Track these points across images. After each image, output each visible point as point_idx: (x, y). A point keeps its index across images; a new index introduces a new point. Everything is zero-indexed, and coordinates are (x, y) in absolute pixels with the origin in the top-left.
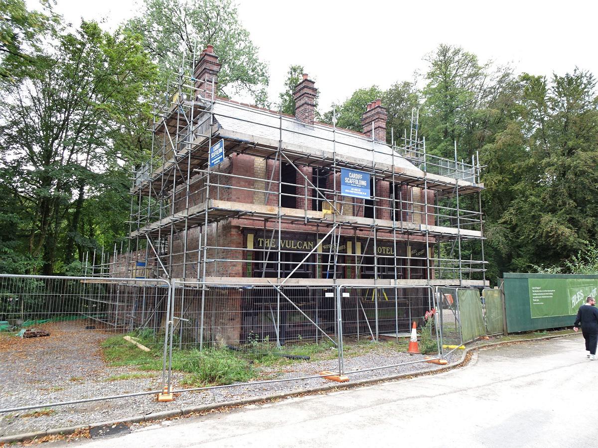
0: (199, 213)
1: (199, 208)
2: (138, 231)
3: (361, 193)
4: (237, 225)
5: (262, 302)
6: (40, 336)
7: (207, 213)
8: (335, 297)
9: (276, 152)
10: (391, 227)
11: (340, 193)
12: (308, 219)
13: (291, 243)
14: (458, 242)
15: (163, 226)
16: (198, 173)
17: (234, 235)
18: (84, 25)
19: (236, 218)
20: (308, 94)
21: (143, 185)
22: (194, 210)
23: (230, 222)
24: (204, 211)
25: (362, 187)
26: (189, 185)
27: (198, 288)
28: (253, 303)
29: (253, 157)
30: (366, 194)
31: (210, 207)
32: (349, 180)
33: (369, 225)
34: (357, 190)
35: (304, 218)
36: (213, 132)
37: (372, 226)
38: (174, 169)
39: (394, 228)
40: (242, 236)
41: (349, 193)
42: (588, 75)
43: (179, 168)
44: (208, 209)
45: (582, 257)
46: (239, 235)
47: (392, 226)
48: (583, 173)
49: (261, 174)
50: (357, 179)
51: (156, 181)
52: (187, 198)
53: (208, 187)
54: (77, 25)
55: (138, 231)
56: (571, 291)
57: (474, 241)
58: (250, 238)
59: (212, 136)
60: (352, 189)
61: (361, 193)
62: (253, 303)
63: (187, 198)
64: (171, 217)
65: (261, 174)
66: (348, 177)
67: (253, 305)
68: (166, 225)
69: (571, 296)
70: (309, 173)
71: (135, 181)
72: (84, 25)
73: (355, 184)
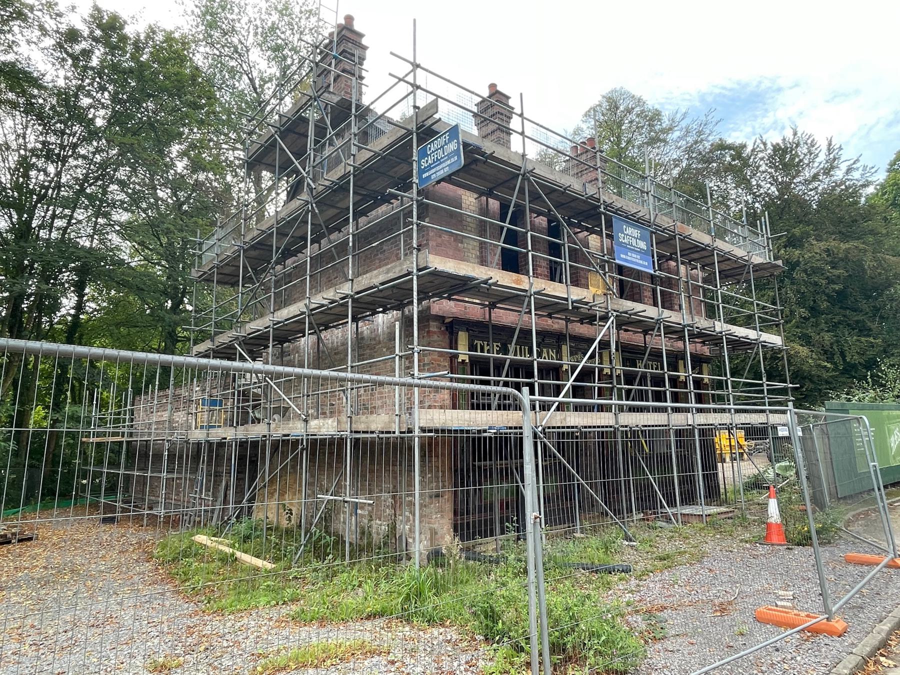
0: (383, 284)
1: (387, 273)
2: (213, 341)
3: (641, 262)
4: (440, 314)
5: (491, 460)
6: (20, 541)
7: (415, 278)
8: (792, 434)
9: (518, 175)
10: (680, 324)
11: (614, 260)
12: (572, 303)
13: (525, 349)
14: (757, 354)
15: (279, 322)
16: (395, 197)
17: (435, 333)
18: (97, 15)
19: (445, 298)
20: (502, 114)
21: (219, 260)
22: (322, 298)
23: (429, 308)
24: (409, 273)
25: (641, 252)
26: (311, 258)
27: (397, 434)
28: (474, 460)
29: (461, 191)
30: (647, 264)
31: (422, 266)
32: (624, 239)
33: (652, 319)
34: (635, 256)
35: (566, 299)
36: (420, 120)
37: (658, 320)
38: (307, 213)
39: (685, 326)
40: (447, 337)
41: (626, 261)
42: (809, 142)
43: (317, 211)
44: (419, 270)
45: (873, 380)
46: (443, 333)
47: (682, 322)
48: (816, 271)
49: (471, 225)
50: (634, 237)
51: (252, 246)
52: (350, 260)
53: (415, 227)
54: (85, 10)
55: (213, 341)
56: (889, 430)
57: (773, 354)
58: (463, 338)
59: (418, 129)
60: (629, 254)
61: (641, 262)
62: (474, 460)
63: (350, 260)
64: (270, 317)
65: (471, 225)
66: (623, 232)
67: (474, 466)
68: (286, 320)
69: (890, 438)
70: (543, 228)
71: (200, 257)
72: (97, 15)
73: (632, 245)
